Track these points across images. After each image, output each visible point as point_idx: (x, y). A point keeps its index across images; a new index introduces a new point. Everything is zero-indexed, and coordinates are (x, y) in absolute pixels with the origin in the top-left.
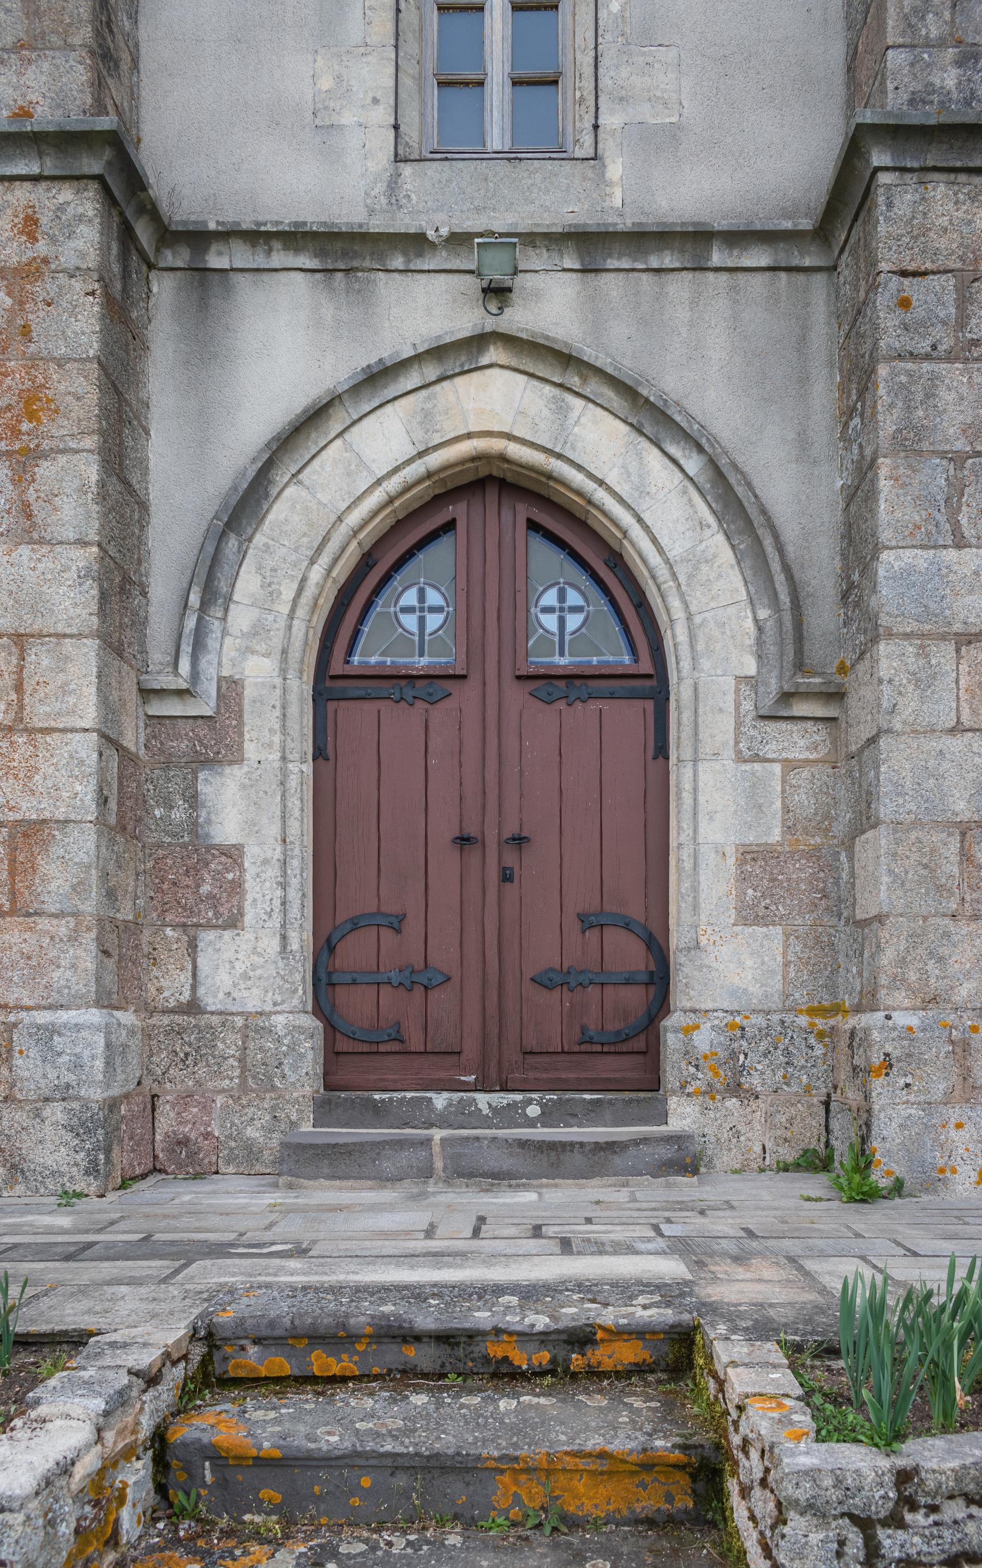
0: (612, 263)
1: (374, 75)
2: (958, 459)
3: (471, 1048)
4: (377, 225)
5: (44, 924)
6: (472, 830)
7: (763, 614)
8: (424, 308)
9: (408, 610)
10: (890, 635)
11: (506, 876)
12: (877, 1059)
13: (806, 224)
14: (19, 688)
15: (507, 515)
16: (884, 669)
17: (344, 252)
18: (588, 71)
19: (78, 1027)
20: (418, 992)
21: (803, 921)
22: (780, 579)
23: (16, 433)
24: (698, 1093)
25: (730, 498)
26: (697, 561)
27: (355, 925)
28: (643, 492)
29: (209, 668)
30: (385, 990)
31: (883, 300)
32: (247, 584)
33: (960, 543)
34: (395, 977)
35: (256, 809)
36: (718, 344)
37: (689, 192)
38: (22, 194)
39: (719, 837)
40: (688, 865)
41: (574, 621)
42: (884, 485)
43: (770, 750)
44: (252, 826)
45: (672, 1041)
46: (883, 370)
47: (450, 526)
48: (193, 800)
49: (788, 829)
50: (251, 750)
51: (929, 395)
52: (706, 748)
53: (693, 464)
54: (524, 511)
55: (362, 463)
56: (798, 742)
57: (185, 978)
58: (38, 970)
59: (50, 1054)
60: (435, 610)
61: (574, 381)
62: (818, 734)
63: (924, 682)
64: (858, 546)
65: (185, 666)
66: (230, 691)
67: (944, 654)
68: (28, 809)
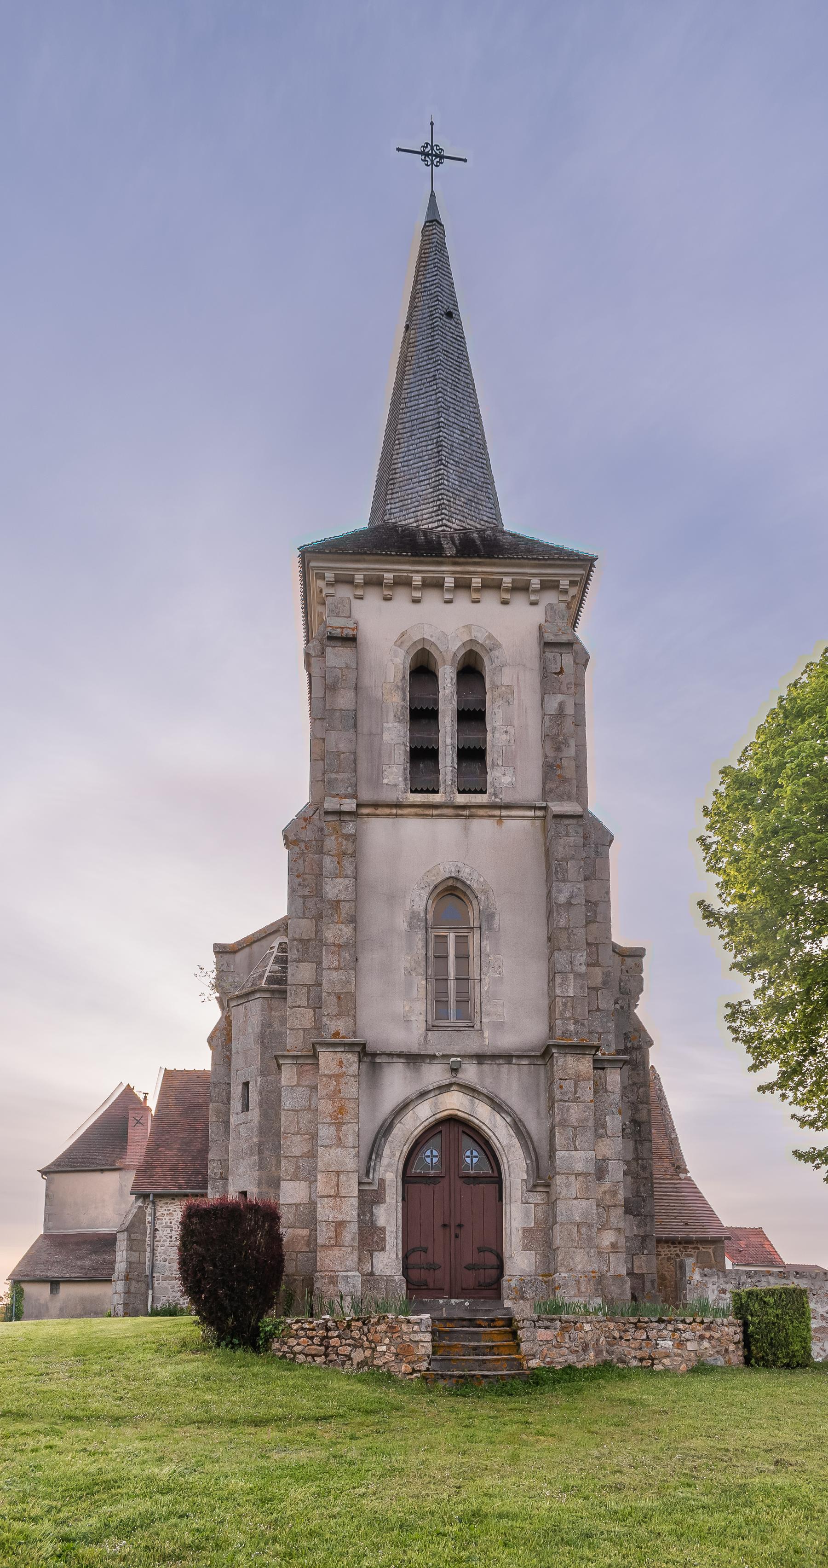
0: (486, 1062)
1: (420, 1006)
2: (575, 1128)
3: (447, 1288)
4: (423, 1053)
5: (344, 1249)
6: (447, 1223)
7: (528, 1162)
8: (435, 1074)
9: (428, 1156)
10: (559, 1173)
11: (457, 1236)
12: (557, 1285)
13: (538, 1054)
14: (338, 1185)
15: (456, 1128)
16: (558, 1183)
17: (413, 1059)
18: (479, 1005)
19: (354, 1276)
20: (432, 1271)
21: (540, 1250)
22: (532, 1153)
23: (337, 1118)
24: (512, 1299)
25: (519, 1128)
26: (510, 1146)
27: (414, 1250)
28: (495, 1126)
29: (377, 1177)
30: (422, 1271)
31: (556, 1086)
32: (386, 1152)
33: (576, 1150)
34: (425, 1267)
35: (389, 1216)
36: (515, 1085)
37: (508, 1041)
38: (339, 1055)
39: (517, 1225)
40: (508, 1233)
41: (475, 1160)
42: (557, 1134)
43: (530, 1201)
44: (388, 1221)
45: (505, 1284)
46: (556, 1105)
47: (441, 1132)
48: (372, 1214)
49: (536, 1223)
50: (387, 1199)
51: (568, 1111)
52: (513, 1200)
53: (509, 1119)
54: (461, 1129)
55: (418, 1117)
56: (538, 1198)
57: (369, 1265)
58: (342, 1261)
60: (436, 1156)
61: (476, 1095)
62: (544, 1196)
63: (568, 1186)
64: (552, 1150)
65: (371, 1176)
66: (382, 1182)
67: (572, 1179)
68: (340, 1218)
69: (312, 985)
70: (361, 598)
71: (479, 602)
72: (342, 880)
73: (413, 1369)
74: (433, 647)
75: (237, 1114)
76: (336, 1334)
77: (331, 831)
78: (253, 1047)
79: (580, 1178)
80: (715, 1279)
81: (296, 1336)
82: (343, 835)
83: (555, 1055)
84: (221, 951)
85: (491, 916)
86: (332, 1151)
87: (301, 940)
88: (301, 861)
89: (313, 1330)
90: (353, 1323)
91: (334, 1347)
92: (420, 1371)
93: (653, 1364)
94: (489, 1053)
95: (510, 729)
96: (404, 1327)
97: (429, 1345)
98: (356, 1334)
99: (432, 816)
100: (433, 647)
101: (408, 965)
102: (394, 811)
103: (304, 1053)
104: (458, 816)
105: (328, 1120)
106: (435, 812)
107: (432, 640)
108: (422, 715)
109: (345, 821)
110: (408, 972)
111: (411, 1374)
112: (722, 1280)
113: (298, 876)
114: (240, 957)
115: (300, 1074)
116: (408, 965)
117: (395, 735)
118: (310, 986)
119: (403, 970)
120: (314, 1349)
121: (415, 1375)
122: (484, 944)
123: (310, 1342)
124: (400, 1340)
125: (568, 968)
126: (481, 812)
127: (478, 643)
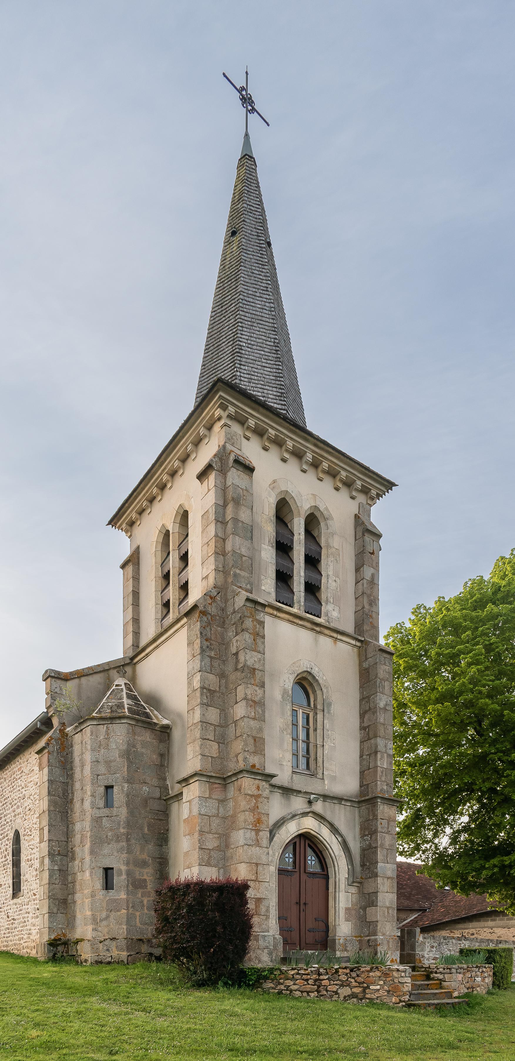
2: (388, 850)
5: (261, 917)
7: (349, 867)
8: (299, 804)
14: (257, 873)
17: (287, 791)
23: (256, 826)
25: (345, 845)
37: (338, 789)
38: (257, 782)
49: (352, 905)
52: (341, 890)
53: (340, 839)
59: (265, 940)
61: (322, 821)
62: (356, 888)
63: (383, 884)
68: (259, 896)
69: (218, 726)
70: (248, 439)
71: (321, 480)
72: (256, 654)
73: (400, 1000)
74: (292, 500)
75: (99, 808)
76: (327, 977)
77: (249, 615)
78: (118, 759)
79: (389, 880)
80: (429, 940)
81: (293, 979)
82: (257, 620)
83: (379, 803)
84: (53, 676)
85: (330, 705)
86: (253, 849)
87: (209, 690)
88: (208, 629)
89: (308, 974)
90: (340, 970)
91: (325, 986)
92: (404, 1001)
93: (473, 991)
94: (332, 795)
95: (337, 579)
96: (395, 974)
97: (410, 985)
98: (343, 978)
99: (297, 624)
100: (292, 500)
101: (282, 726)
102: (275, 613)
103: (218, 775)
104: (312, 630)
105: (251, 827)
106: (301, 622)
107: (293, 495)
108: (283, 548)
109: (258, 610)
110: (282, 731)
111: (399, 1003)
112: (432, 941)
113: (207, 640)
114: (71, 685)
115: (211, 790)
116: (282, 726)
117: (268, 555)
118: (216, 726)
119: (278, 728)
120: (308, 988)
121: (401, 1004)
122: (325, 722)
123: (306, 983)
124: (391, 982)
125: (384, 750)
126: (327, 632)
127: (320, 510)
